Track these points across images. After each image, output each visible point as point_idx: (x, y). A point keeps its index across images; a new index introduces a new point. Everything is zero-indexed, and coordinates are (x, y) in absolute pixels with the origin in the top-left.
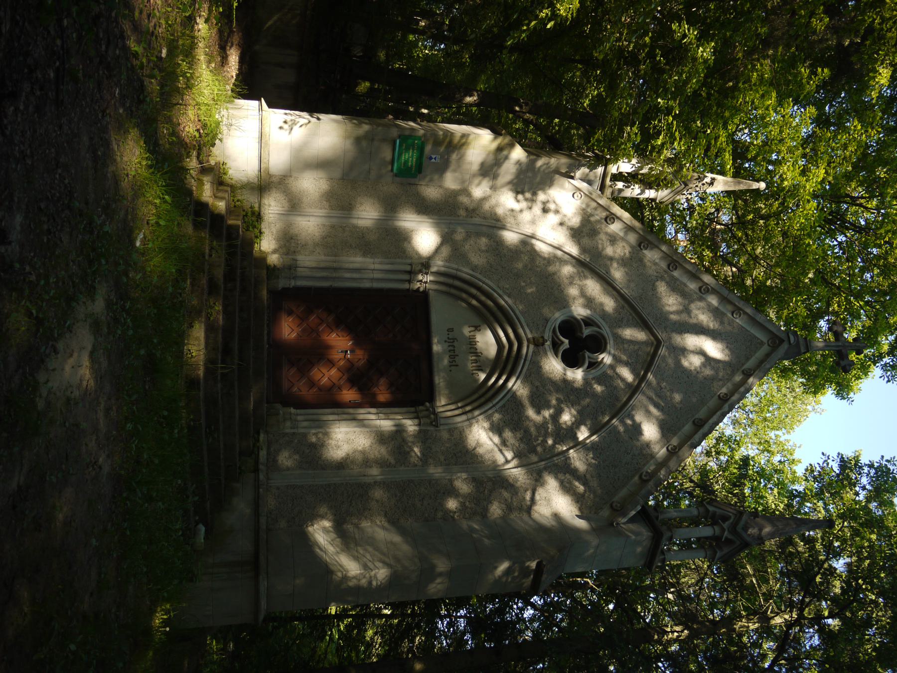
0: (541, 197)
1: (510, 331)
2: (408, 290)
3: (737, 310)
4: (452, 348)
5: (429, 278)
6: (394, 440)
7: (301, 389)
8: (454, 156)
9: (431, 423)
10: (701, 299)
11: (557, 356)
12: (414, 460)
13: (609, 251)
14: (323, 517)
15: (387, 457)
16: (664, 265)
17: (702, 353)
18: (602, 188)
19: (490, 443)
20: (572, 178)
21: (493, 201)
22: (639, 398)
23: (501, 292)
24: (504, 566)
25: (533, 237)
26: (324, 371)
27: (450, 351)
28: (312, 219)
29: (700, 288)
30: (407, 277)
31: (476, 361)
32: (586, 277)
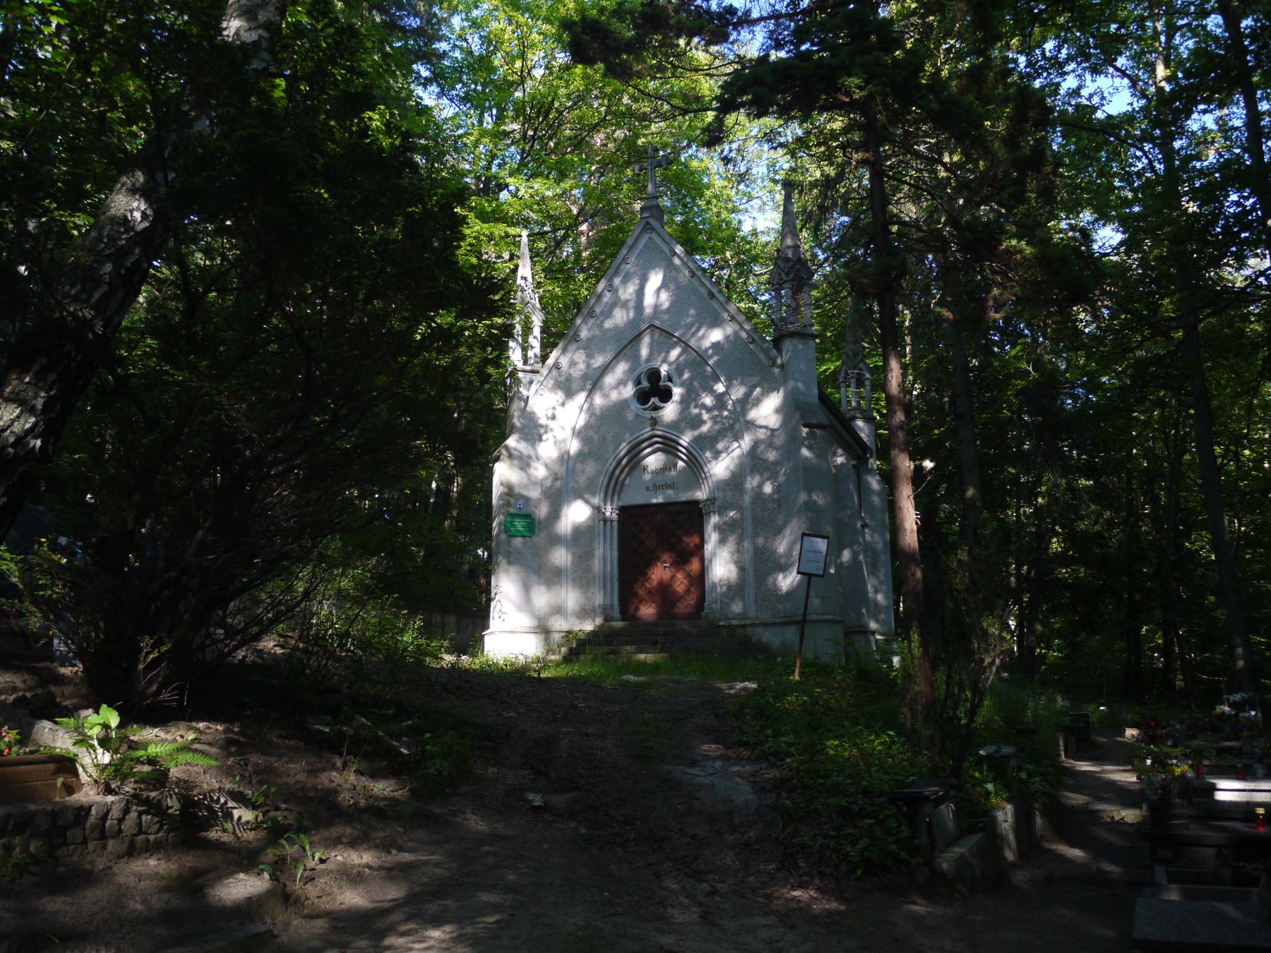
0: (543, 421)
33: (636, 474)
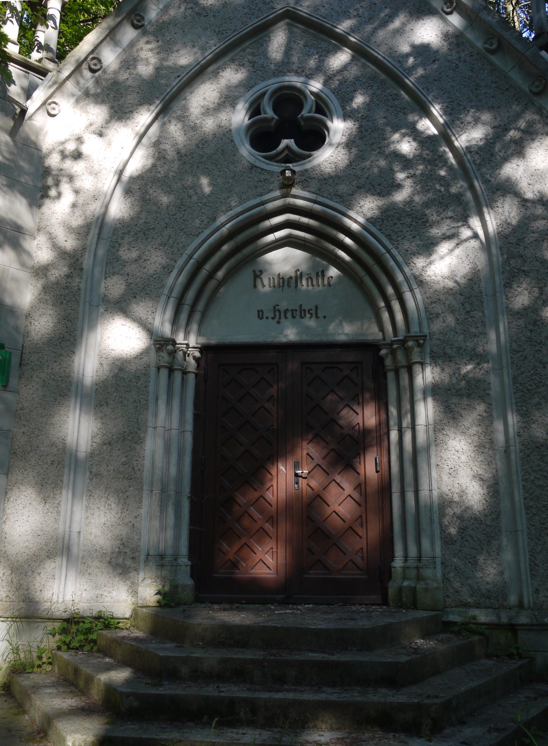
0: (54, 161)
4: (289, 314)
9: (419, 345)
11: (310, 156)
13: (145, 70)
27: (294, 317)
30: (178, 376)
33: (246, 276)
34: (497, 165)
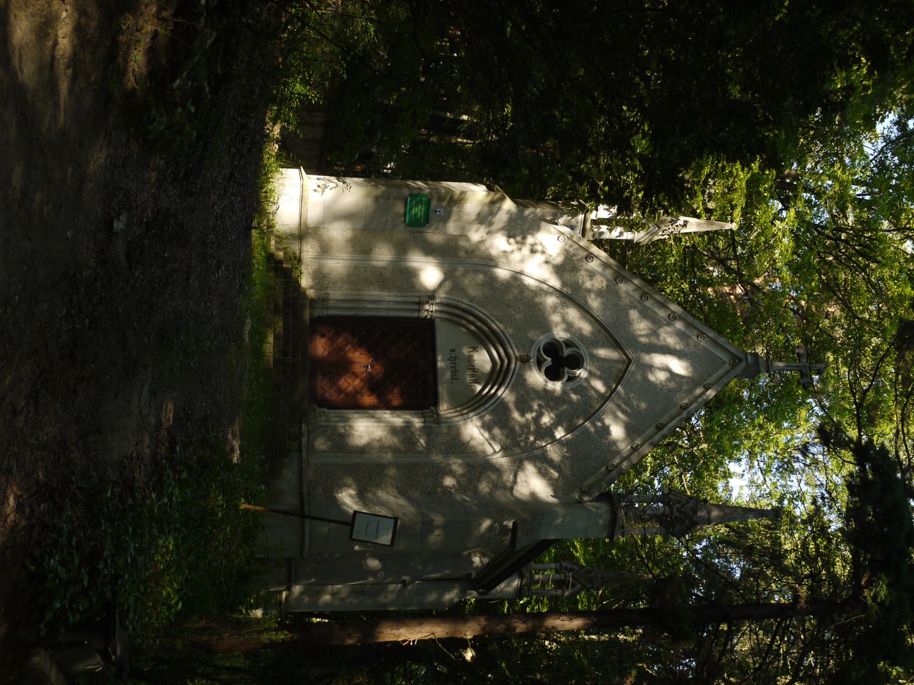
0: (530, 240)
1: (501, 350)
2: (418, 318)
3: (701, 334)
5: (434, 308)
6: (404, 433)
7: (331, 394)
8: (455, 209)
10: (669, 324)
12: (420, 448)
14: (349, 487)
15: (399, 446)
16: (637, 295)
17: (667, 369)
18: (583, 234)
19: (481, 438)
20: (556, 224)
21: (487, 244)
22: (610, 405)
23: (493, 319)
24: (486, 523)
25: (521, 273)
26: (349, 381)
28: (340, 262)
29: (669, 316)
30: (416, 307)
31: (473, 376)
32: (568, 307)
34: (292, 160)
